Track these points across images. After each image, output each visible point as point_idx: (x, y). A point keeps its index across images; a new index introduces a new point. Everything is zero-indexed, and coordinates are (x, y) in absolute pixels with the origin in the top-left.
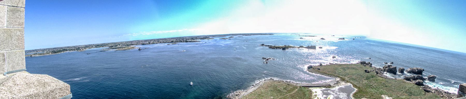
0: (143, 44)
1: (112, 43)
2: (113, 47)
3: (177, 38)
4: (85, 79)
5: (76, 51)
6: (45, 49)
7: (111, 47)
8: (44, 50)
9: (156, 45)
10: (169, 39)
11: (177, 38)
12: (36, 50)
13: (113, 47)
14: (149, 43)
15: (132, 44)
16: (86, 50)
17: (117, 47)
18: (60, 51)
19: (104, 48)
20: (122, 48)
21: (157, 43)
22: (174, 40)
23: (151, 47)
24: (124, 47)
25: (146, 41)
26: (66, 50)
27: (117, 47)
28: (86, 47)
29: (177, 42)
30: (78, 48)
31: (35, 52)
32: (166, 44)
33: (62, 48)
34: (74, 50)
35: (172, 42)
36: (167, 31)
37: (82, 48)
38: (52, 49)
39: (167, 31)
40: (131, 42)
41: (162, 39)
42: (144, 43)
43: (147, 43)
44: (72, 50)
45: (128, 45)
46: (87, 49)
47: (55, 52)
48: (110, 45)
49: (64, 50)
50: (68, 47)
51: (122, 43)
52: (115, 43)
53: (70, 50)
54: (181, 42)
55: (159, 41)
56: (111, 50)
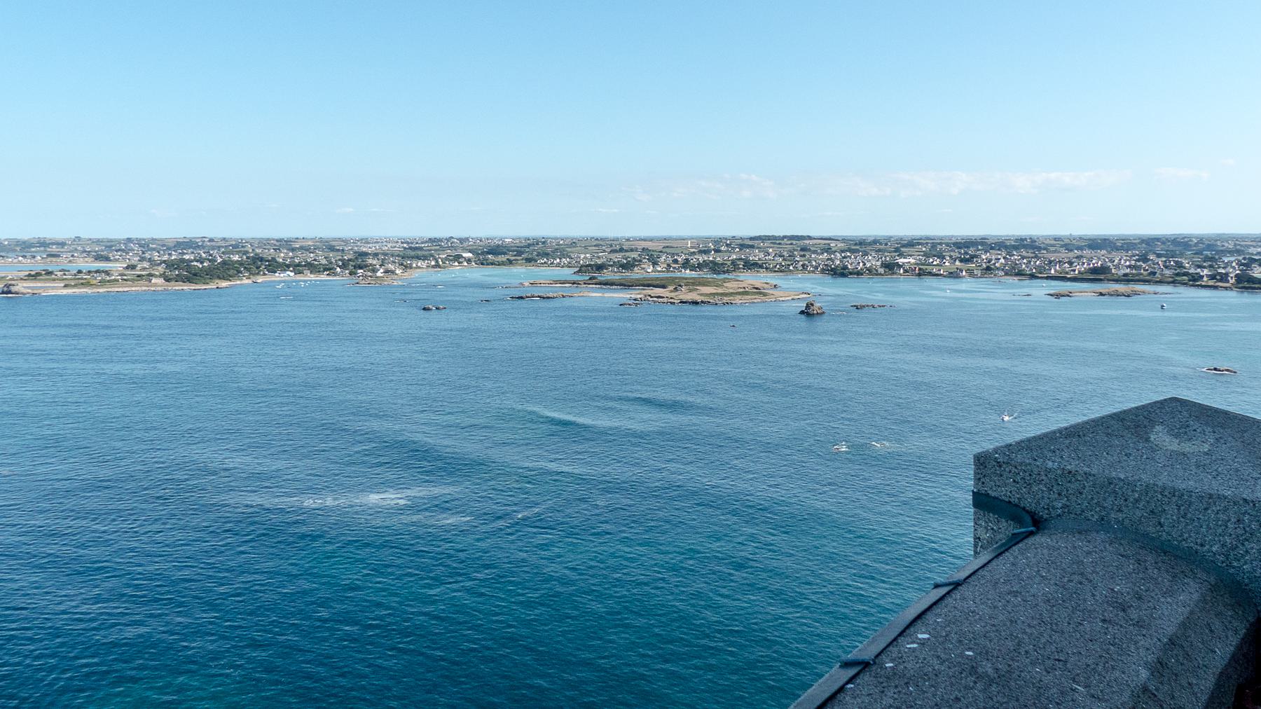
0: (840, 273)
1: (599, 243)
2: (607, 275)
3: (1150, 242)
4: (442, 506)
5: (341, 278)
6: (110, 245)
7: (593, 272)
8: (104, 250)
9: (941, 291)
10: (1068, 244)
11: (1145, 247)
12: (43, 244)
13: (607, 275)
14: (890, 267)
15: (750, 266)
16: (414, 275)
17: (637, 274)
18: (226, 270)
19: (545, 273)
20: (678, 284)
21: (954, 275)
22: (1122, 263)
23: (903, 301)
24: (693, 284)
25: (860, 246)
26: (273, 266)
27: (637, 274)
28: (412, 253)
29: (1152, 279)
30: (357, 261)
31: (39, 264)
32: (1040, 290)
33: (237, 246)
34: (329, 269)
35: (1098, 274)
36: (1119, 312)
37: (383, 256)
38: (165, 246)
39: (1119, 312)
40: (746, 244)
41: (1000, 245)
42: (844, 259)
43: (873, 261)
44: (313, 267)
45: (715, 267)
46: (421, 272)
47: (193, 276)
48: (585, 258)
49: (256, 261)
50: (286, 244)
51: (669, 246)
52: (617, 246)
53: (297, 268)
54: (1194, 281)
55: (970, 255)
56: (595, 295)
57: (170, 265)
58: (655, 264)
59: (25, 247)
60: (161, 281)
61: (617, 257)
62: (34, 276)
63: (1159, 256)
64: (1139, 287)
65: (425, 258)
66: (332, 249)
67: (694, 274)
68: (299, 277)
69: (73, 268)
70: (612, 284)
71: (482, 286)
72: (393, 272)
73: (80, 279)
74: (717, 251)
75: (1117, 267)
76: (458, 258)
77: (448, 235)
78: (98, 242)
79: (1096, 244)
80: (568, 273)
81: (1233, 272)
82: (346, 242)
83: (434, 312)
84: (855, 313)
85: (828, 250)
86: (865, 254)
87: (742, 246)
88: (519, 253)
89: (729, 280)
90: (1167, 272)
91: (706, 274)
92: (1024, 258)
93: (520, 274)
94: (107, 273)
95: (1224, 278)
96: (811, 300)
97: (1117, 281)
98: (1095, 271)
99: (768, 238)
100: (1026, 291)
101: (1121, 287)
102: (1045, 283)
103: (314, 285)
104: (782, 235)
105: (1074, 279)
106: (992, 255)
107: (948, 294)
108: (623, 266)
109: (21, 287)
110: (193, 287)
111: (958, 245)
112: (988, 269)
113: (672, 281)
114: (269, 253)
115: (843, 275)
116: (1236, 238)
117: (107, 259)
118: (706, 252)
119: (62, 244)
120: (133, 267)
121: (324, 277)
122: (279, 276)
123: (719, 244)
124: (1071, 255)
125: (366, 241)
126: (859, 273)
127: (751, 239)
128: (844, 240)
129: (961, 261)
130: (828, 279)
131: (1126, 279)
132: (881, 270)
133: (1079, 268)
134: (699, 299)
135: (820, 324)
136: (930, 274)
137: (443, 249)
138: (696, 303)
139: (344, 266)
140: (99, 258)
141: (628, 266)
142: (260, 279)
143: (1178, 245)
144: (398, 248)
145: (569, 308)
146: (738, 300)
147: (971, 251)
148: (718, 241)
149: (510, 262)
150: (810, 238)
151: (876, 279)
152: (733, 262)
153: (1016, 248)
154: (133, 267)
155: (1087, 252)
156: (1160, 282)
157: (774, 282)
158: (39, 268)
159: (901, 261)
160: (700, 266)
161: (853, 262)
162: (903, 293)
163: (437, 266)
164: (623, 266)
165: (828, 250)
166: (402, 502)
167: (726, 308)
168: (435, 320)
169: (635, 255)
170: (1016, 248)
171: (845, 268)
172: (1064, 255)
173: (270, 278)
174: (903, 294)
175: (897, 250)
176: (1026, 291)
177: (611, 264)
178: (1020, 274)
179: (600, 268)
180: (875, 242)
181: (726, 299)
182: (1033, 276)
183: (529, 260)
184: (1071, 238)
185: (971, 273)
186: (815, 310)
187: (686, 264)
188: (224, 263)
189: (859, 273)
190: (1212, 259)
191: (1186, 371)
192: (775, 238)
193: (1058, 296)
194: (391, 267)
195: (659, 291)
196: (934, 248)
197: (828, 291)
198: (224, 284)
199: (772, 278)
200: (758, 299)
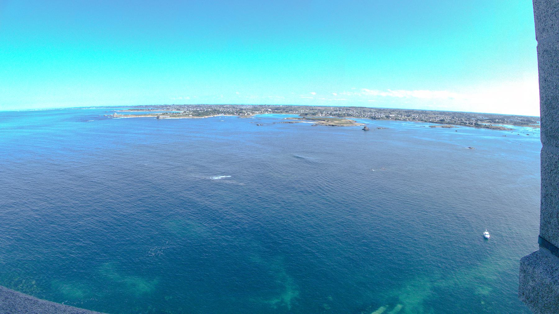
0: (374, 118)
1: (306, 107)
2: (308, 117)
3: (455, 113)
5: (236, 116)
7: (304, 116)
8: (179, 107)
10: (434, 113)
12: (166, 106)
13: (308, 117)
14: (388, 117)
15: (349, 115)
16: (255, 115)
17: (316, 117)
18: (207, 113)
19: (291, 116)
21: (405, 120)
22: (448, 119)
24: (332, 120)
25: (380, 110)
26: (219, 112)
27: (316, 117)
28: (255, 109)
31: (165, 111)
32: (427, 125)
33: (210, 106)
34: (233, 113)
35: (442, 122)
37: (247, 110)
38: (193, 107)
40: (348, 109)
43: (383, 115)
44: (229, 113)
45: (339, 115)
46: (257, 114)
47: (199, 115)
48: (302, 111)
52: (311, 108)
53: (225, 113)
54: (465, 124)
55: (409, 115)
57: (194, 112)
58: (322, 114)
59: (162, 107)
61: (311, 112)
64: (452, 126)
65: (258, 111)
66: (234, 108)
71: (274, 119)
73: (173, 115)
76: (267, 111)
78: (178, 105)
81: (474, 122)
82: (237, 105)
84: (378, 130)
85: (371, 111)
86: (381, 113)
87: (347, 109)
88: (284, 110)
92: (424, 116)
94: (179, 113)
95: (472, 124)
98: (441, 120)
101: (448, 125)
103: (228, 117)
105: (436, 123)
108: (313, 114)
116: (474, 114)
117: (180, 110)
118: (337, 111)
119: (170, 106)
120: (185, 112)
122: (220, 115)
125: (243, 105)
131: (449, 123)
137: (263, 108)
142: (215, 116)
143: (461, 114)
144: (251, 107)
146: (345, 125)
147: (409, 114)
148: (340, 108)
160: (335, 115)
161: (378, 115)
162: (393, 125)
164: (313, 114)
165: (371, 111)
172: (433, 116)
178: (422, 120)
179: (306, 114)
182: (425, 121)
183: (286, 112)
184: (435, 111)
186: (367, 129)
187: (331, 114)
191: (66, 289)
195: (323, 122)
196: (399, 112)
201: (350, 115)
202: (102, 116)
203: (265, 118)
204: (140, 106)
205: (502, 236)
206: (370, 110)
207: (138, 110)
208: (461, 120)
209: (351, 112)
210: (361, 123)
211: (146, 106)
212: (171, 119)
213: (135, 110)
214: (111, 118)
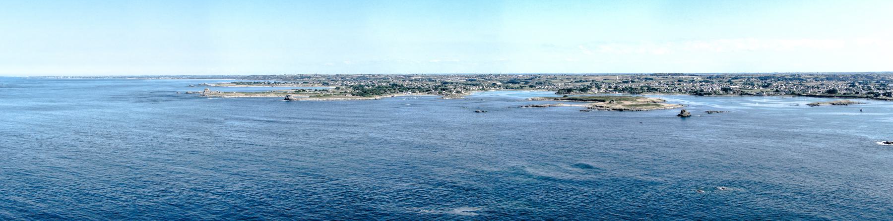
0: (699, 94)
1: (569, 77)
2: (573, 95)
3: (855, 76)
5: (434, 95)
6: (329, 78)
8: (326, 80)
9: (751, 103)
10: (816, 77)
12: (302, 77)
13: (573, 95)
14: (726, 90)
15: (651, 90)
17: (589, 94)
18: (379, 90)
19: (539, 94)
21: (759, 95)
22: (842, 88)
24: (619, 100)
25: (710, 79)
26: (402, 89)
27: (589, 94)
28: (471, 82)
30: (441, 86)
32: (803, 102)
33: (385, 78)
35: (831, 93)
42: (700, 87)
43: (717, 88)
44: (420, 89)
45: (632, 91)
46: (475, 93)
47: (365, 93)
48: (561, 85)
49: (395, 86)
50: (408, 77)
51: (607, 78)
52: (578, 79)
53: (413, 90)
54: (876, 96)
55: (767, 84)
56: (567, 105)
57: (355, 88)
58: (599, 88)
59: (295, 79)
60: (350, 95)
61: (578, 85)
62: (298, 92)
63: (860, 83)
64: (851, 100)
65: (476, 85)
66: (430, 80)
67: (620, 94)
68: (414, 94)
69: (313, 89)
70: (576, 99)
72: (460, 92)
73: (316, 93)
74: (633, 82)
75: (841, 89)
77: (488, 73)
78: (324, 76)
79: (830, 77)
80: (552, 94)
83: (481, 114)
85: (693, 81)
86: (713, 83)
87: (646, 79)
88: (526, 83)
89: (639, 98)
90: (864, 92)
91: (627, 94)
92: (794, 85)
93: (526, 94)
96: (684, 108)
97: (840, 97)
98: (830, 92)
99: (660, 75)
100: (797, 102)
102: (806, 98)
103: (421, 98)
104: (668, 72)
105: (820, 96)
106: (779, 83)
107: (757, 105)
109: (292, 97)
110: (364, 98)
111: (761, 78)
112: (777, 91)
113: (609, 97)
114: (400, 82)
115: (701, 95)
117: (328, 84)
119: (309, 77)
120: (338, 88)
121: (426, 94)
123: (634, 78)
124: (818, 83)
125: (448, 76)
126: (709, 94)
127: (652, 75)
128: (701, 76)
129: (763, 87)
130: (693, 97)
131: (845, 96)
132: (721, 92)
133: (823, 90)
134: (623, 108)
135: (688, 121)
136: (747, 94)
137: (486, 80)
138: (621, 110)
139: (436, 89)
140: (324, 84)
141: (583, 90)
142: (395, 95)
143: (868, 78)
145: (556, 113)
146: (644, 108)
147: (768, 81)
148: (633, 76)
149: (522, 87)
150: (683, 74)
151: (719, 97)
152: (642, 88)
153: (791, 79)
154: (338, 88)
155: (825, 82)
156: (861, 97)
157: (664, 99)
158: (300, 88)
159: (732, 87)
160: (623, 90)
161: (706, 88)
163: (483, 89)
165: (693, 81)
166: (474, 214)
167: (639, 113)
168: (482, 118)
169: (588, 84)
170: (791, 79)
171: (702, 91)
172: (815, 84)
173: (400, 94)
174: (731, 104)
175: (729, 81)
176: (797, 102)
177: (574, 89)
178: (793, 93)
179: (569, 91)
180: (718, 77)
181: (637, 108)
182: (799, 95)
183: (531, 87)
184: (818, 74)
185: (768, 93)
187: (616, 89)
188: (379, 87)
189: (709, 94)
190: (884, 85)
192: (664, 74)
193: (812, 105)
194: (459, 90)
197: (693, 103)
198: (378, 97)
199: (663, 97)
200: (655, 108)
201: (653, 89)
202: (190, 92)
203: (489, 99)
204: (254, 77)
205: (362, 87)
206: (692, 78)
207: (249, 83)
208: (869, 88)
209: (654, 84)
210: (673, 103)
211: (265, 77)
212: (311, 102)
213: (243, 83)
214: (203, 97)
